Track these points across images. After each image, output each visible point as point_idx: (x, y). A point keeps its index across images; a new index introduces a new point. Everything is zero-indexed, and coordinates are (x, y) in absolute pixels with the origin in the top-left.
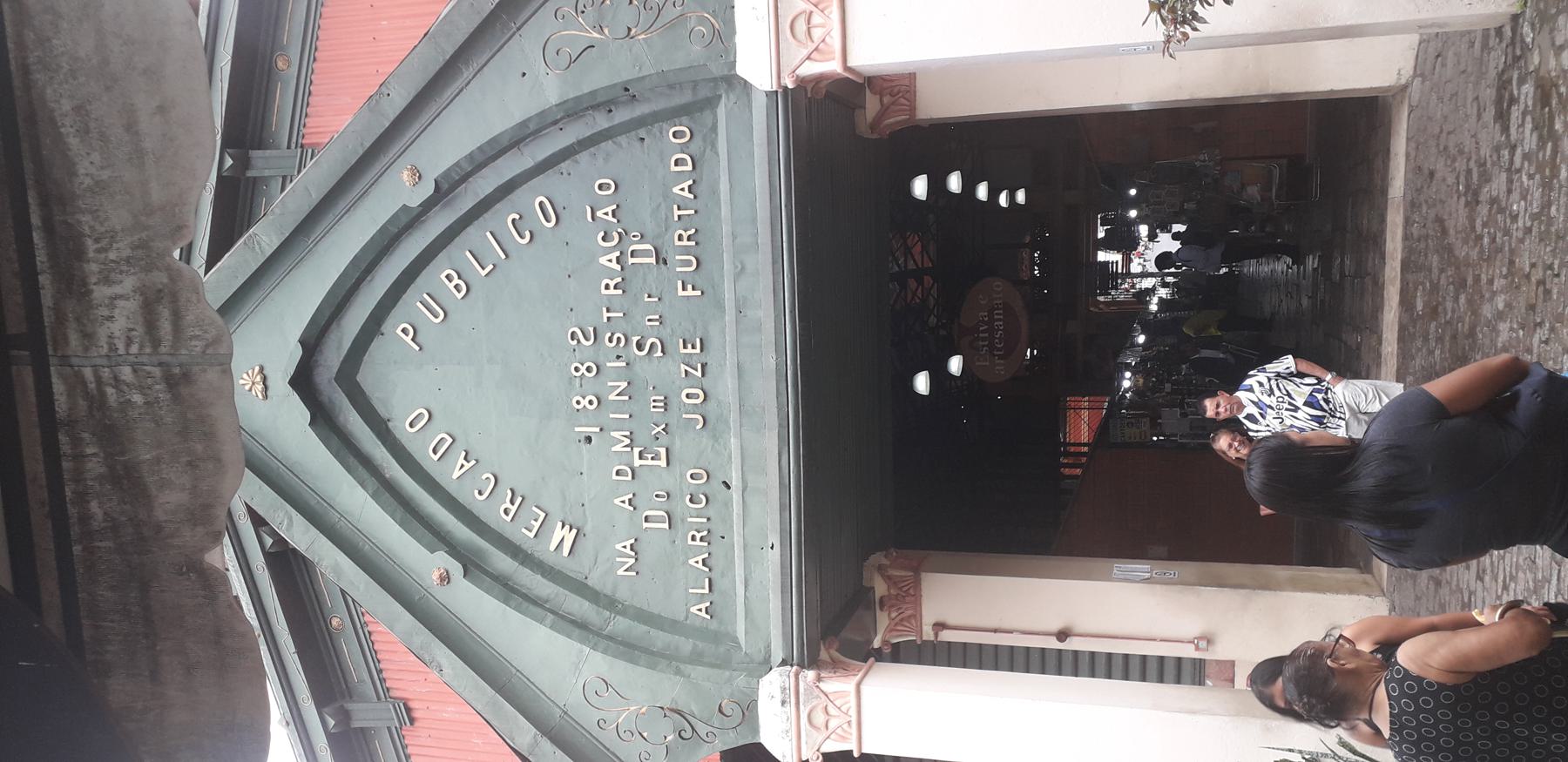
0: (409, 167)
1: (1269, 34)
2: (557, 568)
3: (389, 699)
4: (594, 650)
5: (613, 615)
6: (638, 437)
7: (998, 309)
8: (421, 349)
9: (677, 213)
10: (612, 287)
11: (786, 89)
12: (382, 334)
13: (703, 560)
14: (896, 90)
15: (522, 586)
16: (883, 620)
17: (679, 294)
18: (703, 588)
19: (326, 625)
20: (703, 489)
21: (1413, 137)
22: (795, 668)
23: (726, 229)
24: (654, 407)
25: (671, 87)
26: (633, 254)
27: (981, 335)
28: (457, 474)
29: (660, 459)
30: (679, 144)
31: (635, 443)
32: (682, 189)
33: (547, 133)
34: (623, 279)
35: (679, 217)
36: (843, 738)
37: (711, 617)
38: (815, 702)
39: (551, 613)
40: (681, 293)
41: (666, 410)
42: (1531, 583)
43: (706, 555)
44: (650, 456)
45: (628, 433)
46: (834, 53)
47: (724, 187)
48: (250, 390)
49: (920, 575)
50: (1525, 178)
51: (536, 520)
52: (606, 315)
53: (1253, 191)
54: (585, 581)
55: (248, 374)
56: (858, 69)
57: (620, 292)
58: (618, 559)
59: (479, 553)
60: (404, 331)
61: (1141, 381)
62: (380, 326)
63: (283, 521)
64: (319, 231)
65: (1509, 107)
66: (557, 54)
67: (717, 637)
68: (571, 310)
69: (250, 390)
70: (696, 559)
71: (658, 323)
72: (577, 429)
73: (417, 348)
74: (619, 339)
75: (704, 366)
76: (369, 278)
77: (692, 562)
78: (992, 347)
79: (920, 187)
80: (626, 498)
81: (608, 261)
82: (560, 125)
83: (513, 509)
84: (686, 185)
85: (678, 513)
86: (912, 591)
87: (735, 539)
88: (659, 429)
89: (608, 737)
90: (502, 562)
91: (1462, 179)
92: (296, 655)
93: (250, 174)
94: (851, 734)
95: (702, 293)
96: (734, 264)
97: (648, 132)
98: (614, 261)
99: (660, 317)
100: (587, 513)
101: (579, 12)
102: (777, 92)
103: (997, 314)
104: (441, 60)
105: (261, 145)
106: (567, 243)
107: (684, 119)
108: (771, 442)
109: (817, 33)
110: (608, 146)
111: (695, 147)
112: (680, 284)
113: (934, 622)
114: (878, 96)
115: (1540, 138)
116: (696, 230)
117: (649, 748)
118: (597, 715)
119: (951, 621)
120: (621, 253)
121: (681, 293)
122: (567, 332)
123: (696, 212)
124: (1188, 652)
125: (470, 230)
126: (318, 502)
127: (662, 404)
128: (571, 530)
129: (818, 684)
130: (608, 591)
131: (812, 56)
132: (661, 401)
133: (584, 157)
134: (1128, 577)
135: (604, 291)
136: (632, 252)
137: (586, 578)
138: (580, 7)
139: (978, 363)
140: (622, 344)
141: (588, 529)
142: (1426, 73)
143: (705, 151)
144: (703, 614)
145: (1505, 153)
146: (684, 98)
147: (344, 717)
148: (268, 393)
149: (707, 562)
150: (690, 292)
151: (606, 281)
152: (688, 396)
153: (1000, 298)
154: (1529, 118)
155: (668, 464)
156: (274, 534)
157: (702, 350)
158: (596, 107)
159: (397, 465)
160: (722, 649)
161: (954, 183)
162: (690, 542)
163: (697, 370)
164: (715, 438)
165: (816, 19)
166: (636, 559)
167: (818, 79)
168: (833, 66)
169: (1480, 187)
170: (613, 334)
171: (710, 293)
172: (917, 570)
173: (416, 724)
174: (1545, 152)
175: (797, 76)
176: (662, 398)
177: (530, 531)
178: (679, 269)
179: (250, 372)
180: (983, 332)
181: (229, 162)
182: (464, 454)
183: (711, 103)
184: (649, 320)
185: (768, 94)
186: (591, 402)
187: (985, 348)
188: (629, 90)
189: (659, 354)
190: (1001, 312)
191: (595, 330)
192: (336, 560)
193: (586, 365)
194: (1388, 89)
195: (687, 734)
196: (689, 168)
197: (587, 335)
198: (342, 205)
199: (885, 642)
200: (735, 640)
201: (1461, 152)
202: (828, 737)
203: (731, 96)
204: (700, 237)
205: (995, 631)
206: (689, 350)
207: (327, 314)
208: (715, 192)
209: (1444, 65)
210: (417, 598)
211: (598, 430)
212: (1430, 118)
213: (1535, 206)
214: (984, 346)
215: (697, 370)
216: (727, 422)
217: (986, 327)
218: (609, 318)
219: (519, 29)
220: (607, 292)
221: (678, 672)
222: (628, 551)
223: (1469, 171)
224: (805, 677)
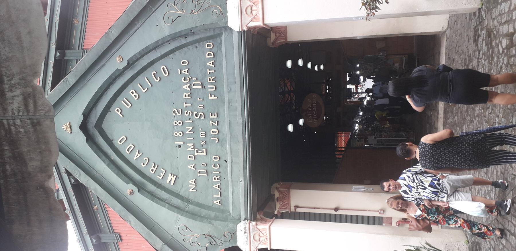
1: (403, 14)
2: (169, 189)
3: (114, 233)
4: (182, 216)
5: (188, 204)
6: (196, 146)
8: (123, 116)
9: (208, 71)
10: (187, 96)
11: (244, 31)
12: (110, 112)
14: (281, 31)
16: (278, 205)
18: (218, 195)
19: (93, 209)
20: (218, 162)
21: (448, 48)
22: (249, 221)
23: (225, 77)
24: (201, 135)
25: (206, 30)
26: (194, 85)
28: (135, 158)
29: (204, 153)
30: (209, 49)
31: (195, 148)
32: (210, 64)
33: (165, 45)
34: (191, 93)
35: (209, 73)
36: (265, 244)
37: (221, 205)
38: (255, 232)
39: (167, 204)
40: (210, 98)
41: (205, 136)
42: (486, 191)
43: (219, 184)
44: (200, 152)
45: (193, 144)
46: (260, 19)
47: (224, 63)
48: (66, 130)
49: (290, 190)
50: (483, 61)
51: (162, 173)
52: (185, 105)
53: (397, 65)
54: (179, 193)
56: (268, 25)
57: (190, 97)
58: (190, 186)
59: (143, 184)
60: (117, 110)
61: (361, 127)
62: (109, 109)
63: (77, 174)
64: (89, 77)
65: (478, 38)
66: (168, 19)
67: (223, 211)
68: (174, 103)
69: (66, 130)
70: (216, 186)
71: (202, 108)
72: (176, 143)
73: (122, 116)
74: (189, 113)
75: (218, 122)
76: (106, 93)
77: (214, 186)
78: (313, 116)
79: (289, 64)
80: (192, 166)
81: (186, 87)
82: (169, 42)
83: (155, 169)
84: (211, 62)
85: (210, 170)
86: (287, 196)
87: (229, 178)
88: (203, 143)
89: (187, 245)
90: (151, 187)
91: (463, 61)
92: (82, 219)
93: (65, 58)
95: (217, 98)
96: (228, 88)
97: (199, 45)
98: (188, 87)
99: (203, 106)
100: (179, 171)
101: (175, 5)
102: (241, 32)
103: (314, 105)
104: (129, 20)
105: (69, 49)
106: (172, 81)
107: (211, 40)
108: (240, 147)
109: (254, 13)
110: (185, 49)
111: (214, 50)
112: (210, 95)
113: (294, 205)
114: (275, 34)
115: (488, 48)
116: (215, 77)
117: (201, 248)
118: (183, 237)
119: (300, 205)
120: (190, 85)
121: (210, 98)
123: (215, 71)
124: (377, 214)
125: (139, 77)
127: (204, 134)
128: (174, 176)
129: (256, 226)
130: (187, 197)
131: (253, 20)
132: (204, 133)
133: (177, 53)
134: (357, 190)
135: (184, 97)
137: (179, 192)
138: (176, 3)
141: (180, 176)
142: (452, 27)
143: (218, 51)
144: (218, 204)
145: (477, 53)
146: (211, 33)
147: (99, 239)
148: (72, 131)
149: (220, 186)
150: (213, 97)
151: (185, 94)
154: (484, 42)
155: (206, 154)
156: (74, 178)
157: (217, 117)
158: (181, 36)
159: (115, 155)
160: (224, 215)
161: (300, 62)
162: (214, 180)
163: (215, 123)
164: (222, 146)
165: (254, 8)
166: (196, 186)
167: (255, 28)
168: (260, 23)
169: (469, 64)
170: (187, 111)
172: (289, 189)
173: (123, 241)
174: (489, 52)
175: (248, 27)
176: (204, 132)
177: (160, 177)
178: (209, 90)
179: (66, 124)
181: (58, 54)
182: (138, 151)
183: (219, 35)
184: (200, 107)
185: (238, 32)
186: (180, 134)
189: (203, 118)
190: (316, 104)
191: (181, 110)
192: (95, 187)
194: (440, 32)
195: (213, 243)
196: (213, 56)
198: (97, 68)
200: (229, 212)
201: (463, 52)
202: (260, 244)
203: (226, 33)
204: (216, 79)
205: (314, 208)
206: (213, 117)
208: (221, 65)
209: (457, 25)
210: (123, 199)
211: (183, 143)
212: (453, 42)
213: (486, 70)
214: (310, 116)
215: (215, 123)
216: (226, 141)
218: (186, 106)
219: (155, 10)
220: (185, 97)
221: (210, 223)
222: (193, 183)
223: (465, 59)
224: (252, 224)
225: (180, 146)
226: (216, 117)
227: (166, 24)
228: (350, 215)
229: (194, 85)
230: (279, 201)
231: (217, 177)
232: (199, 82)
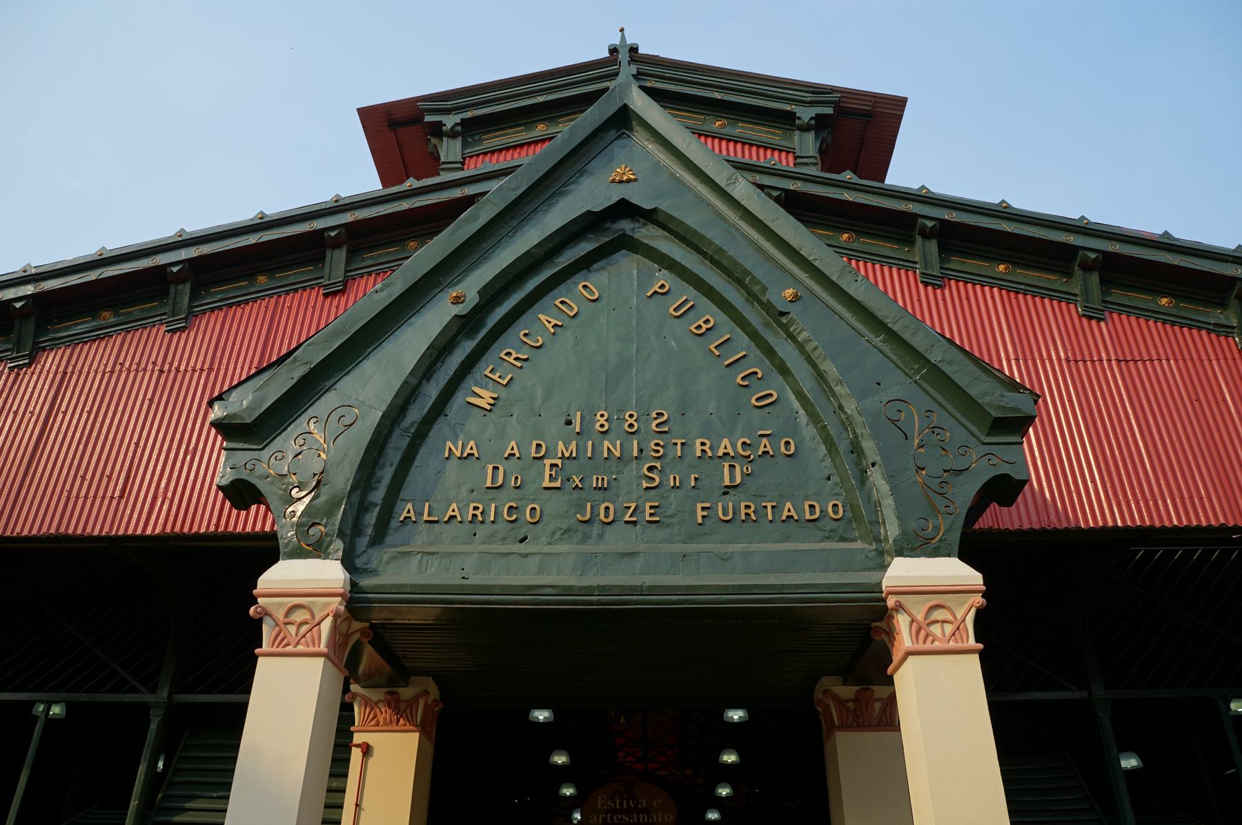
0: (799, 294)
7: (648, 818)
9: (679, 442)
11: (884, 600)
13: (410, 518)
15: (443, 362)
17: (698, 504)
20: (522, 518)
22: (349, 595)
24: (597, 479)
26: (732, 467)
27: (625, 801)
31: (567, 462)
32: (789, 511)
39: (418, 383)
40: (699, 506)
44: (553, 473)
51: (500, 377)
55: (629, 171)
60: (662, 286)
62: (666, 269)
74: (658, 451)
75: (634, 523)
78: (614, 811)
81: (725, 446)
83: (511, 360)
88: (577, 482)
94: (278, 647)
97: (836, 484)
98: (726, 451)
102: (882, 592)
103: (644, 817)
112: (708, 505)
119: (372, 762)
122: (663, 410)
126: (525, 213)
127: (600, 485)
132: (603, 484)
136: (734, 466)
138: (937, 431)
139: (600, 798)
140: (653, 454)
143: (824, 531)
150: (700, 513)
152: (607, 508)
153: (657, 819)
155: (546, 488)
167: (891, 633)
168: (905, 638)
170: (662, 446)
171: (699, 532)
180: (628, 804)
182: (560, 324)
184: (675, 478)
186: (602, 426)
187: (613, 805)
188: (873, 467)
189: (645, 485)
190: (646, 820)
193: (635, 423)
196: (808, 517)
197: (661, 426)
199: (355, 695)
206: (648, 511)
207: (678, 229)
208: (786, 538)
210: (441, 279)
214: (615, 804)
217: (632, 806)
222: (468, 451)
225: (569, 423)
226: (648, 518)
227: (884, 403)
228: (341, 819)
229: (732, 467)
230: (388, 697)
231: (481, 513)
232: (738, 480)
